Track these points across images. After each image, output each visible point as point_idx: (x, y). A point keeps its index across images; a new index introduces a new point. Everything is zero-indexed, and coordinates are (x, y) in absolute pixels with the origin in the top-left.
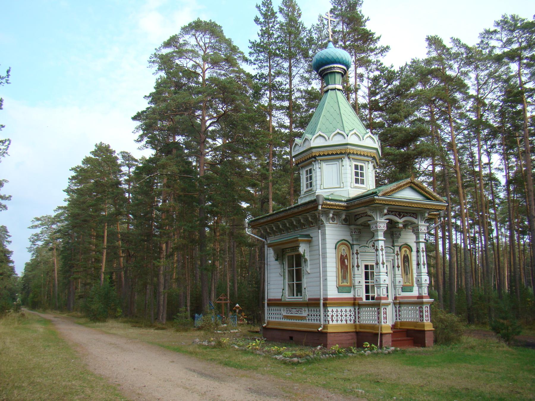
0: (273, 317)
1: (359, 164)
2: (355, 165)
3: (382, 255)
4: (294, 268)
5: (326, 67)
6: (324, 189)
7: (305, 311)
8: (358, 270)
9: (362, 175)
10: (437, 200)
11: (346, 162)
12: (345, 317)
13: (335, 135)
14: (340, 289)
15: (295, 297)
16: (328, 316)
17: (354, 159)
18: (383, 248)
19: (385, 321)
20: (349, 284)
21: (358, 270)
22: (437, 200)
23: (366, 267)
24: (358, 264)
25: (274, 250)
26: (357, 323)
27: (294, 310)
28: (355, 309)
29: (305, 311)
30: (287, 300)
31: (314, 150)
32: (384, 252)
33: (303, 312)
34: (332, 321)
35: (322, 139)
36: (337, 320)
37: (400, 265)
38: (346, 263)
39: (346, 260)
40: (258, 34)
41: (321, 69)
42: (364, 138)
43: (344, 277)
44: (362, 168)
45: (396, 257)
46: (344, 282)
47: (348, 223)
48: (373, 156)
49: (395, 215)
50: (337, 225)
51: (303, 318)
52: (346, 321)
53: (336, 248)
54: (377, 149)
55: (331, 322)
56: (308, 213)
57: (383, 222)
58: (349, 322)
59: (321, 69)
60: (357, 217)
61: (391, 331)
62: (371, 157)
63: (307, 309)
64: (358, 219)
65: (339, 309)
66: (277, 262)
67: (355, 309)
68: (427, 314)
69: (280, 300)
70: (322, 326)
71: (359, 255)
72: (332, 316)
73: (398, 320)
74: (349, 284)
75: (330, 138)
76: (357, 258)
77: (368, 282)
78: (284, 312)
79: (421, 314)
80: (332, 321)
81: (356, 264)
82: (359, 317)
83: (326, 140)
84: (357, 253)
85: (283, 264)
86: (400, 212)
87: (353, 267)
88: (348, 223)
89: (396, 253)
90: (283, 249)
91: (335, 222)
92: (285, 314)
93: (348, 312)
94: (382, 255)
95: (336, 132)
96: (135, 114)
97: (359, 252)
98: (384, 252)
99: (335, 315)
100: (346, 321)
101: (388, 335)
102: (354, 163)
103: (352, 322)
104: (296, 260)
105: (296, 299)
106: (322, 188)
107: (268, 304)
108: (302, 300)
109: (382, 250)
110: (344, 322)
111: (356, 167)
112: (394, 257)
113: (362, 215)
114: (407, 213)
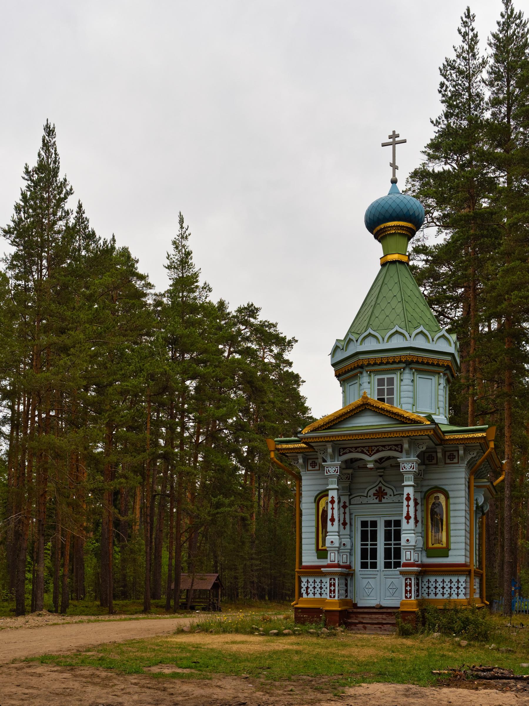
5: (382, 226)
9: (391, 392)
12: (319, 590)
17: (377, 372)
19: (332, 595)
23: (364, 524)
31: (361, 357)
34: (307, 594)
35: (401, 337)
36: (314, 594)
37: (336, 517)
40: (24, 178)
41: (378, 228)
42: (435, 340)
44: (391, 381)
48: (446, 364)
49: (363, 452)
53: (315, 502)
54: (452, 355)
55: (305, 596)
58: (454, 597)
59: (378, 228)
62: (443, 366)
68: (332, 588)
71: (347, 510)
72: (307, 588)
75: (386, 339)
77: (371, 545)
80: (307, 594)
83: (407, 340)
93: (318, 583)
95: (419, 330)
99: (311, 588)
102: (375, 378)
111: (381, 382)
114: (384, 446)
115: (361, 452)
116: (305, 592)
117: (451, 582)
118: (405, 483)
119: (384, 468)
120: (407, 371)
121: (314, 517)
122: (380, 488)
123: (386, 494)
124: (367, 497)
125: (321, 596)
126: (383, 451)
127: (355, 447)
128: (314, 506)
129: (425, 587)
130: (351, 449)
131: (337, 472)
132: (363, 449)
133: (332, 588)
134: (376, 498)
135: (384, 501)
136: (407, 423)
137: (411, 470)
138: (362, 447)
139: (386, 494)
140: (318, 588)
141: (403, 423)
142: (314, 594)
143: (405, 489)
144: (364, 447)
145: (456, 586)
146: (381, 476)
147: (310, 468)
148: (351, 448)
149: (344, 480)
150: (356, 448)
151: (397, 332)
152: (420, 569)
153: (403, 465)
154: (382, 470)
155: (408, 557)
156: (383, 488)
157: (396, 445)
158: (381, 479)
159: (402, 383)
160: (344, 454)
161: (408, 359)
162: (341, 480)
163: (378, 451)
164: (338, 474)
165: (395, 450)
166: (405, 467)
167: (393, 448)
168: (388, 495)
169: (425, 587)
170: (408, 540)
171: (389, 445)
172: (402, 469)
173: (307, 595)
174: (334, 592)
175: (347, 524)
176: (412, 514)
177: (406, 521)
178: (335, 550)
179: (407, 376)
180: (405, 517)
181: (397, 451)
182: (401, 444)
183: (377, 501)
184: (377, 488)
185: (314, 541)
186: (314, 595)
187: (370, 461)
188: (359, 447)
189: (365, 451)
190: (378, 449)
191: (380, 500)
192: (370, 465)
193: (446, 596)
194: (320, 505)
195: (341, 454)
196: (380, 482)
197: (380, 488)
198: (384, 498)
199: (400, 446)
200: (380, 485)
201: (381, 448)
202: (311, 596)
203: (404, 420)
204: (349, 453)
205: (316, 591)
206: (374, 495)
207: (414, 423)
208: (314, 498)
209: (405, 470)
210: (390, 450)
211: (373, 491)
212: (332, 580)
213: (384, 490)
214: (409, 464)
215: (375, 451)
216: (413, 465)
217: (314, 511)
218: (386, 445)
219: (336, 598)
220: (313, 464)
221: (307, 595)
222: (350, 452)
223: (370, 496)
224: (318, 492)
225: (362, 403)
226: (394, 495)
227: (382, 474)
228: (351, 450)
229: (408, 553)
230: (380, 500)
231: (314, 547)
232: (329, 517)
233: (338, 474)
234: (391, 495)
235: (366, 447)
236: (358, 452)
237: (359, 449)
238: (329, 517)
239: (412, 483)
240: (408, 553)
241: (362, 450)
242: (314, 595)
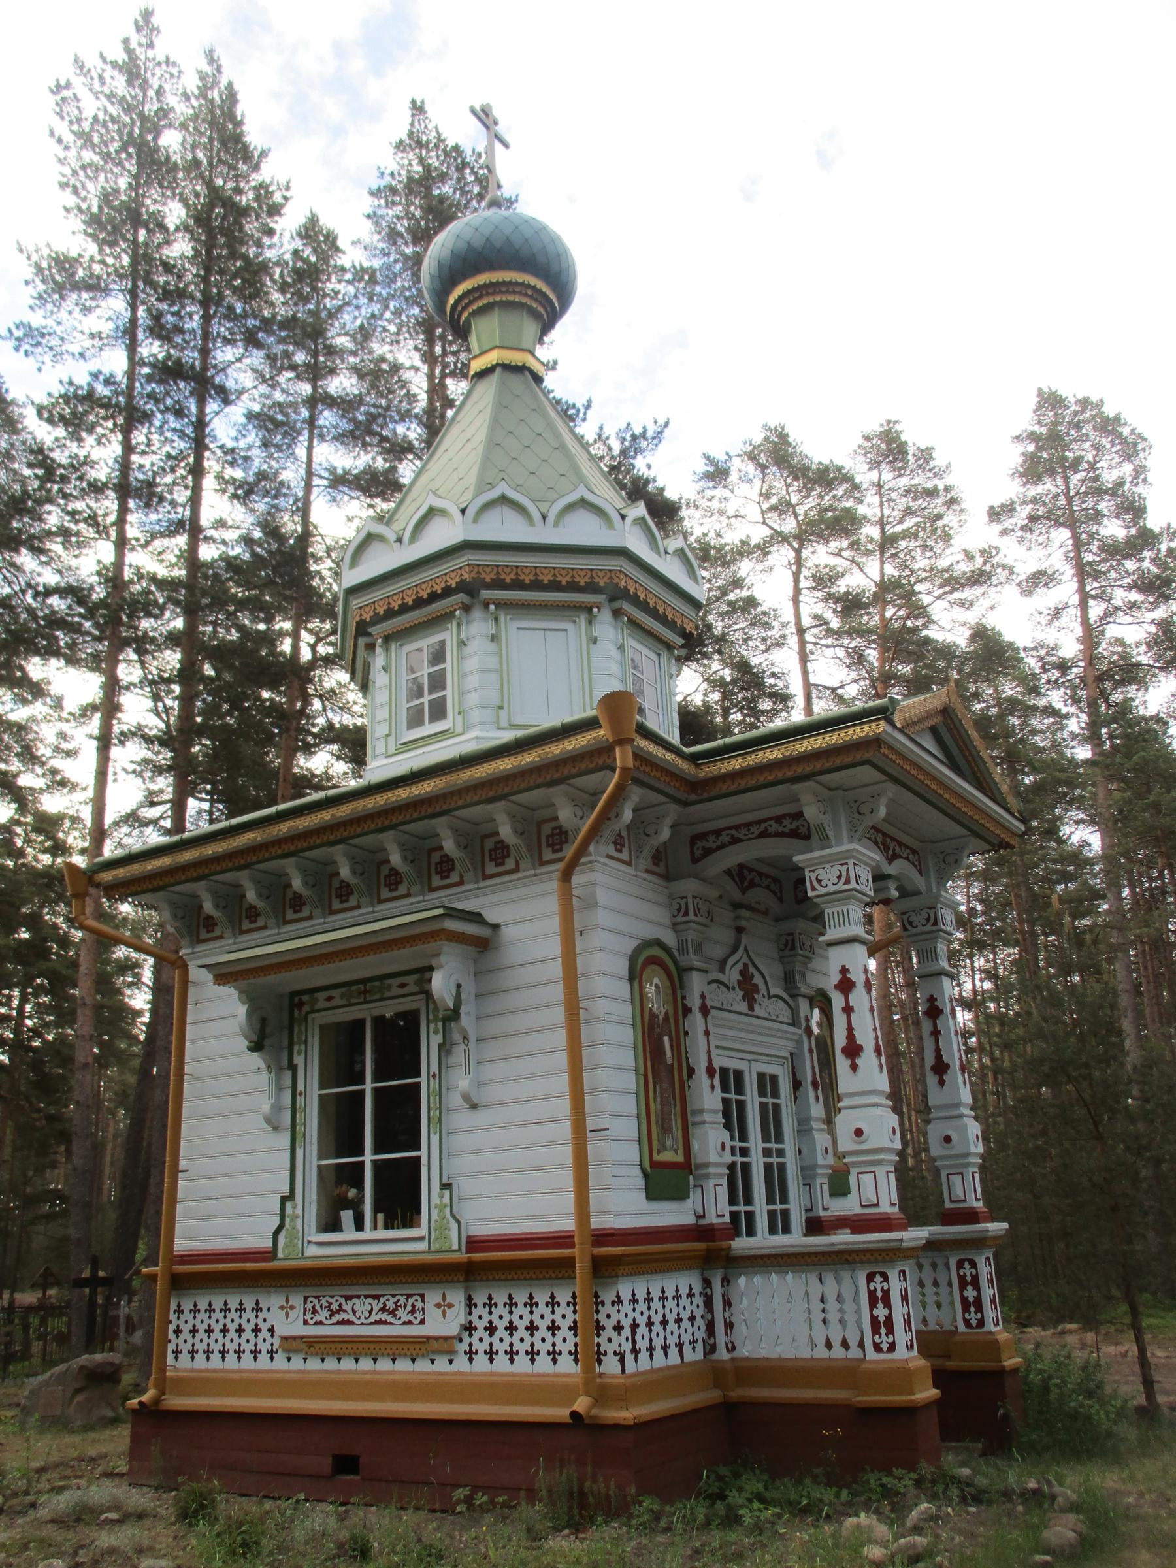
0: (227, 1355)
4: (369, 1086)
7: (444, 1306)
8: (854, 1067)
13: (570, 508)
15: (349, 1234)
16: (573, 1328)
21: (854, 1067)
24: (851, 1036)
25: (251, 998)
26: (723, 1354)
27: (362, 1306)
28: (707, 1283)
29: (444, 1306)
30: (312, 1251)
33: (433, 1314)
35: (509, 513)
39: (666, 1039)
47: (661, 869)
50: (631, 870)
51: (441, 1346)
56: (342, 841)
58: (689, 1356)
60: (711, 842)
63: (457, 1297)
64: (708, 852)
66: (256, 1059)
67: (707, 1283)
69: (271, 1254)
73: (723, 1354)
76: (707, 1033)
78: (285, 1316)
82: (729, 1326)
84: (705, 1011)
85: (293, 1068)
87: (691, 1071)
88: (661, 869)
90: (293, 994)
91: (624, 855)
92: (293, 1325)
95: (573, 497)
96: (236, 87)
97: (709, 1003)
104: (376, 1049)
105: (371, 1241)
106: (504, 722)
108: (423, 1246)
112: (799, 1042)
113: (740, 834)
120: (477, 613)
137: (841, 886)
148: (737, 827)
151: (504, 500)
153: (814, 876)
155: (870, 1195)
159: (467, 651)
166: (819, 882)
167: (712, 838)
171: (759, 822)
172: (813, 889)
174: (890, 1331)
177: (849, 1062)
179: (478, 626)
180: (844, 1050)
195: (698, 853)
204: (731, 844)
209: (821, 891)
210: (764, 834)
212: (878, 1278)
214: (842, 869)
228: (737, 835)
229: (867, 1179)
230: (751, 1008)
232: (840, 1040)
238: (840, 1040)
240: (867, 1179)
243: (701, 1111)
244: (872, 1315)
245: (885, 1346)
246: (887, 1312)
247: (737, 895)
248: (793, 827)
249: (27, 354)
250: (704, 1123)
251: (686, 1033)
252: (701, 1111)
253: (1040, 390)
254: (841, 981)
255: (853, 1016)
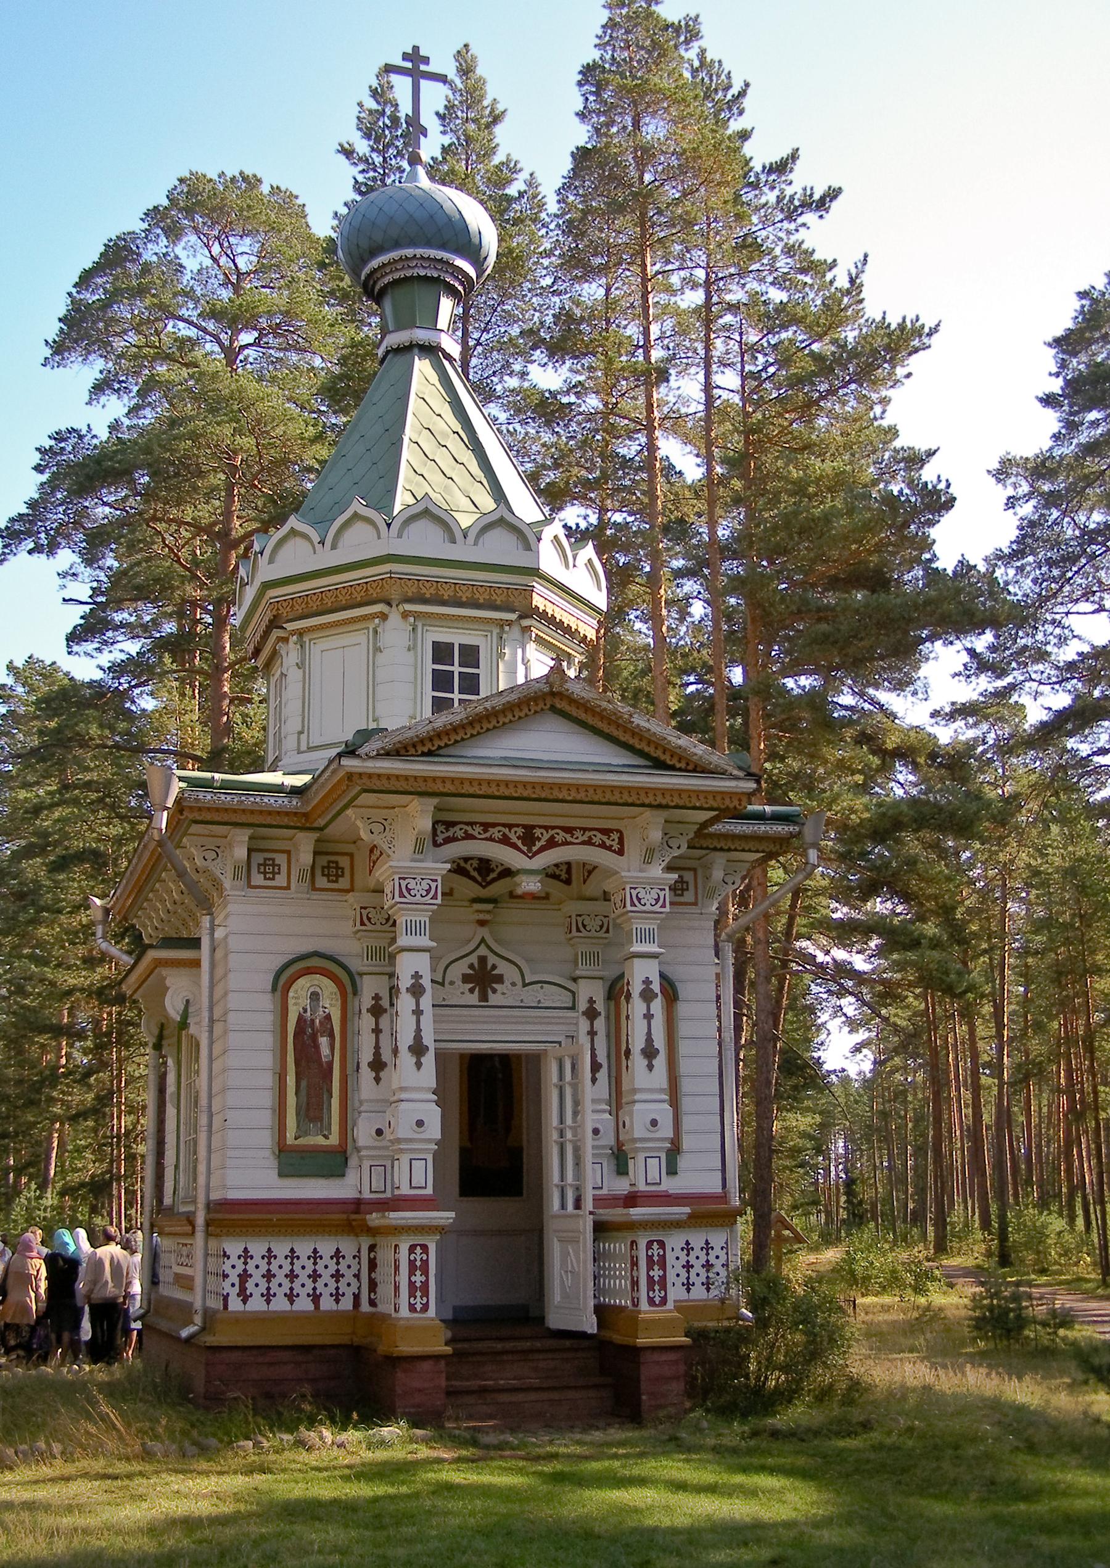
1: (457, 637)
2: (436, 645)
3: (418, 1012)
6: (310, 749)
10: (697, 768)
11: (395, 631)
14: (292, 1160)
18: (426, 982)
20: (334, 1140)
22: (697, 768)
26: (365, 1307)
32: (426, 1002)
34: (245, 1296)
35: (369, 528)
36: (268, 1297)
37: (602, 1058)
38: (325, 1050)
39: (323, 1041)
43: (313, 1111)
44: (470, 655)
45: (584, 1025)
46: (306, 1133)
49: (505, 841)
52: (316, 1298)
53: (274, 989)
55: (235, 1304)
57: (652, 883)
58: (327, 1304)
61: (448, 1349)
65: (281, 1248)
68: (418, 1278)
70: (198, 1319)
72: (244, 1277)
74: (334, 1140)
76: (377, 1031)
79: (656, 1273)
80: (245, 1296)
81: (367, 1056)
86: (528, 829)
89: (583, 1006)
93: (257, 1260)
94: (418, 1012)
98: (426, 1002)
99: (257, 1276)
100: (316, 1298)
101: (426, 1366)
103: (347, 1304)
107: (208, 1224)
109: (417, 990)
110: (304, 1304)
111: (441, 652)
114: (569, 830)
115: (500, 841)
116: (237, 1289)
117: (270, 1256)
118: (637, 948)
119: (493, 901)
121: (268, 1040)
122: (483, 960)
123: (500, 979)
124: (442, 984)
125: (292, 1302)
126: (566, 843)
127: (482, 824)
128: (266, 1002)
129: (349, 1276)
130: (469, 828)
131: (435, 897)
132: (506, 831)
133: (418, 1278)
134: (471, 991)
135: (493, 999)
136: (672, 768)
137: (657, 908)
138: (504, 825)
139: (500, 979)
140: (280, 1277)
141: (659, 765)
142: (268, 1297)
143: (636, 961)
144: (510, 826)
145: (263, 1269)
146: (482, 923)
147: (258, 879)
149: (378, 927)
150: (486, 826)
152: (687, 1210)
154: (490, 906)
156: (492, 960)
157: (606, 832)
158: (484, 932)
160: (448, 840)
161: (424, 590)
162: (369, 927)
163: (552, 844)
164: (439, 901)
165: (603, 846)
168: (507, 983)
169: (349, 1276)
170: (654, 1123)
171: (585, 830)
173: (245, 1301)
174: (425, 1294)
175: (600, 1066)
176: (660, 1042)
177: (414, 1060)
178: (659, 1149)
181: (609, 848)
182: (618, 831)
183: (473, 999)
184: (473, 959)
185: (266, 1118)
186: (268, 1302)
187: (529, 869)
188: (494, 825)
189: (514, 840)
190: (552, 837)
191: (484, 997)
192: (530, 885)
193: (714, 1292)
194: (291, 1002)
195: (440, 840)
196: (483, 940)
197: (483, 960)
198: (494, 991)
199: (615, 836)
200: (483, 951)
201: (561, 836)
202: (256, 1304)
203: (666, 758)
204: (464, 839)
205: (274, 1289)
206: (466, 979)
207: (694, 771)
208: (271, 978)
209: (640, 908)
210: (589, 842)
211: (462, 967)
213: (494, 967)
215: (542, 843)
216: (662, 894)
217: (268, 1020)
218: (575, 829)
219: (432, 1312)
220: (269, 869)
221: (245, 1301)
222: (469, 837)
223: (452, 983)
224: (281, 960)
225: (547, 689)
226: (525, 985)
227: (487, 917)
228: (470, 831)
230: (484, 997)
231: (266, 1139)
233: (439, 901)
234: (514, 984)
235: (518, 826)
236: (491, 839)
237: (495, 832)
239: (424, 941)
241: (504, 835)
242: (268, 1302)
243: (635, 1091)
244: (427, 1277)
245: (418, 1307)
246: (661, 1273)
247: (477, 891)
248: (452, 830)
249: (415, 65)
250: (635, 1102)
251: (628, 1017)
252: (635, 1091)
253: (46, 362)
254: (413, 985)
255: (653, 1022)
